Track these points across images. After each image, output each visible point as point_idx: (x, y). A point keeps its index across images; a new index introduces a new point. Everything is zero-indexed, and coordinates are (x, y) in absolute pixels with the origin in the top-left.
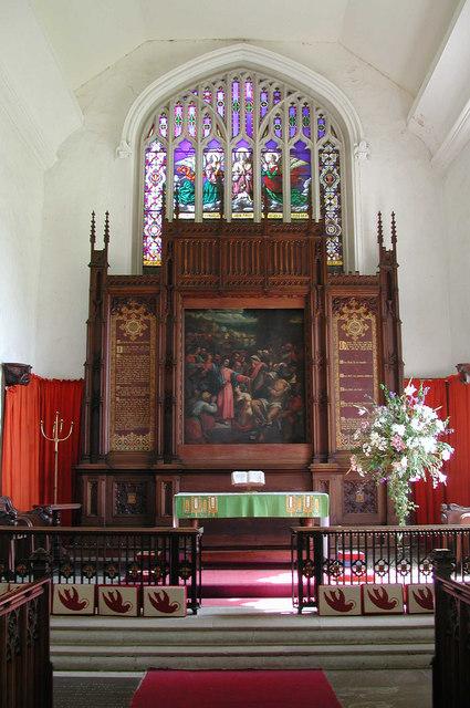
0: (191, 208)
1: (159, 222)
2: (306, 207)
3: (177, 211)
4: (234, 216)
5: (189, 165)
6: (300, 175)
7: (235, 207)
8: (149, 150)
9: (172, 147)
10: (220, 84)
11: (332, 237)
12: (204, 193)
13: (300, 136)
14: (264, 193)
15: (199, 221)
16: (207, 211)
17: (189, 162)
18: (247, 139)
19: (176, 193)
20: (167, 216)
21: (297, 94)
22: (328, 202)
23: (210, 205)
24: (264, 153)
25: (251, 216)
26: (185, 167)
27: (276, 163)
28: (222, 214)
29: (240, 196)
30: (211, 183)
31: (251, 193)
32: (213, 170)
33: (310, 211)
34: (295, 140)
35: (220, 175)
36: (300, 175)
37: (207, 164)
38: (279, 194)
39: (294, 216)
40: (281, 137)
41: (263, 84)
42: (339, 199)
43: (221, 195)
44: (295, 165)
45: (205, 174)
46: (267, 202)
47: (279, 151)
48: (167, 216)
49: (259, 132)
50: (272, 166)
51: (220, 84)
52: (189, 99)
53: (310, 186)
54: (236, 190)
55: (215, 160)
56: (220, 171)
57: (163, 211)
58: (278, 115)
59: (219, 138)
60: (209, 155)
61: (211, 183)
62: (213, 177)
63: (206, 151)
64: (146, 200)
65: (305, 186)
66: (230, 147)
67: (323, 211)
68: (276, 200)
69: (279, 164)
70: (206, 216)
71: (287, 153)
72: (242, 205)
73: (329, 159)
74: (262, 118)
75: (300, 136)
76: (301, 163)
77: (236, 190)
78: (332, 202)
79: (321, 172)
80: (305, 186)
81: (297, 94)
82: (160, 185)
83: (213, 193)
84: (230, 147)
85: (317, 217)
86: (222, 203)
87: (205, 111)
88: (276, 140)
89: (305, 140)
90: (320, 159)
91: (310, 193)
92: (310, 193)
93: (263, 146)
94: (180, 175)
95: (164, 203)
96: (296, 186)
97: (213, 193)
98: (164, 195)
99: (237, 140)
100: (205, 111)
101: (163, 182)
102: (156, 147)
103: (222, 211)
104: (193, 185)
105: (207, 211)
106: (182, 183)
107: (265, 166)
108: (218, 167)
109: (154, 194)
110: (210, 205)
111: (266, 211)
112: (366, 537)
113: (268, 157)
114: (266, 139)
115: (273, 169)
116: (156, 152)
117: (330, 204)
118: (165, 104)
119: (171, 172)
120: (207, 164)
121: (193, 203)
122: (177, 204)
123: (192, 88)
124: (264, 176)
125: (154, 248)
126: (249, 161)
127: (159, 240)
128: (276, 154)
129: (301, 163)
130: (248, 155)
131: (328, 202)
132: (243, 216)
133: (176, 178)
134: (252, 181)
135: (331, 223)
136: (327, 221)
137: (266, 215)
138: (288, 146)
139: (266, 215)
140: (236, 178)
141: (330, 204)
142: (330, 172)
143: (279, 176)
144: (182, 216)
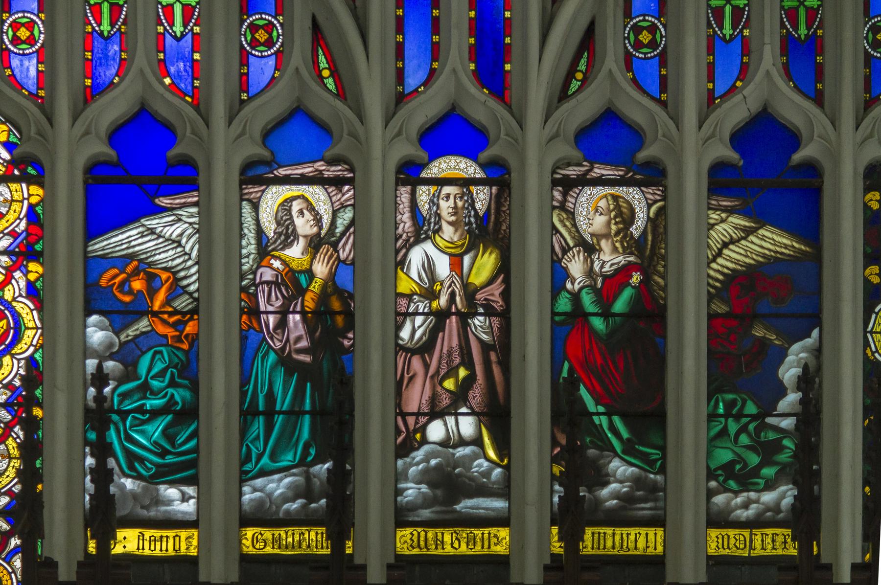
0: (178, 500)
2: (784, 495)
3: (104, 517)
4: (405, 540)
5: (166, 256)
6: (764, 309)
7: (412, 491)
12: (248, 413)
13: (768, 85)
14: (566, 415)
16: (263, 517)
17: (165, 237)
19: (98, 416)
23: (277, 486)
24: (568, 185)
25: (500, 541)
26: (139, 265)
27: (635, 246)
28: (337, 538)
29: (436, 431)
30: (286, 362)
31: (498, 418)
33: (805, 519)
34: (735, 113)
35: (334, 316)
36: (764, 309)
38: (649, 421)
39: (717, 542)
40: (664, 91)
43: (335, 432)
44: (735, 257)
45: (254, 312)
46: (578, 468)
47: (652, 175)
49: (536, 70)
50: (609, 258)
53: (808, 380)
54: (416, 397)
55: (304, 225)
56: (331, 286)
59: (324, 103)
61: (286, 362)
63: (256, 174)
64: (241, 265)
65: (789, 373)
66: (381, 166)
68: (629, 449)
69: (650, 251)
70: (255, 541)
71: (692, 181)
72: (450, 484)
75: (768, 85)
76: (772, 241)
77: (416, 397)
80: (789, 373)
83: (295, 413)
84: (381, 166)
86: (340, 479)
88: (637, 108)
89: (793, 108)
91: (810, 417)
92: (810, 417)
93: (567, 149)
94: (121, 317)
96: (740, 367)
97: (295, 413)
98: (31, 425)
103: (339, 518)
104: (187, 371)
105: (263, 517)
107: (576, 267)
108: (321, 269)
110: (277, 486)
111: (573, 517)
112: (141, 350)
113: (592, 210)
114: (583, 109)
115: (622, 275)
119: (67, 293)
120: (264, 251)
121: (186, 472)
122: (102, 476)
124: (569, 326)
126: (484, 232)
128: (634, 195)
129: (772, 241)
130: (482, 196)
132: (451, 543)
133: (97, 333)
134: (503, 347)
137: (572, 538)
138: (697, 146)
139: (572, 538)
140: (412, 331)
143: (651, 314)
144: (128, 541)
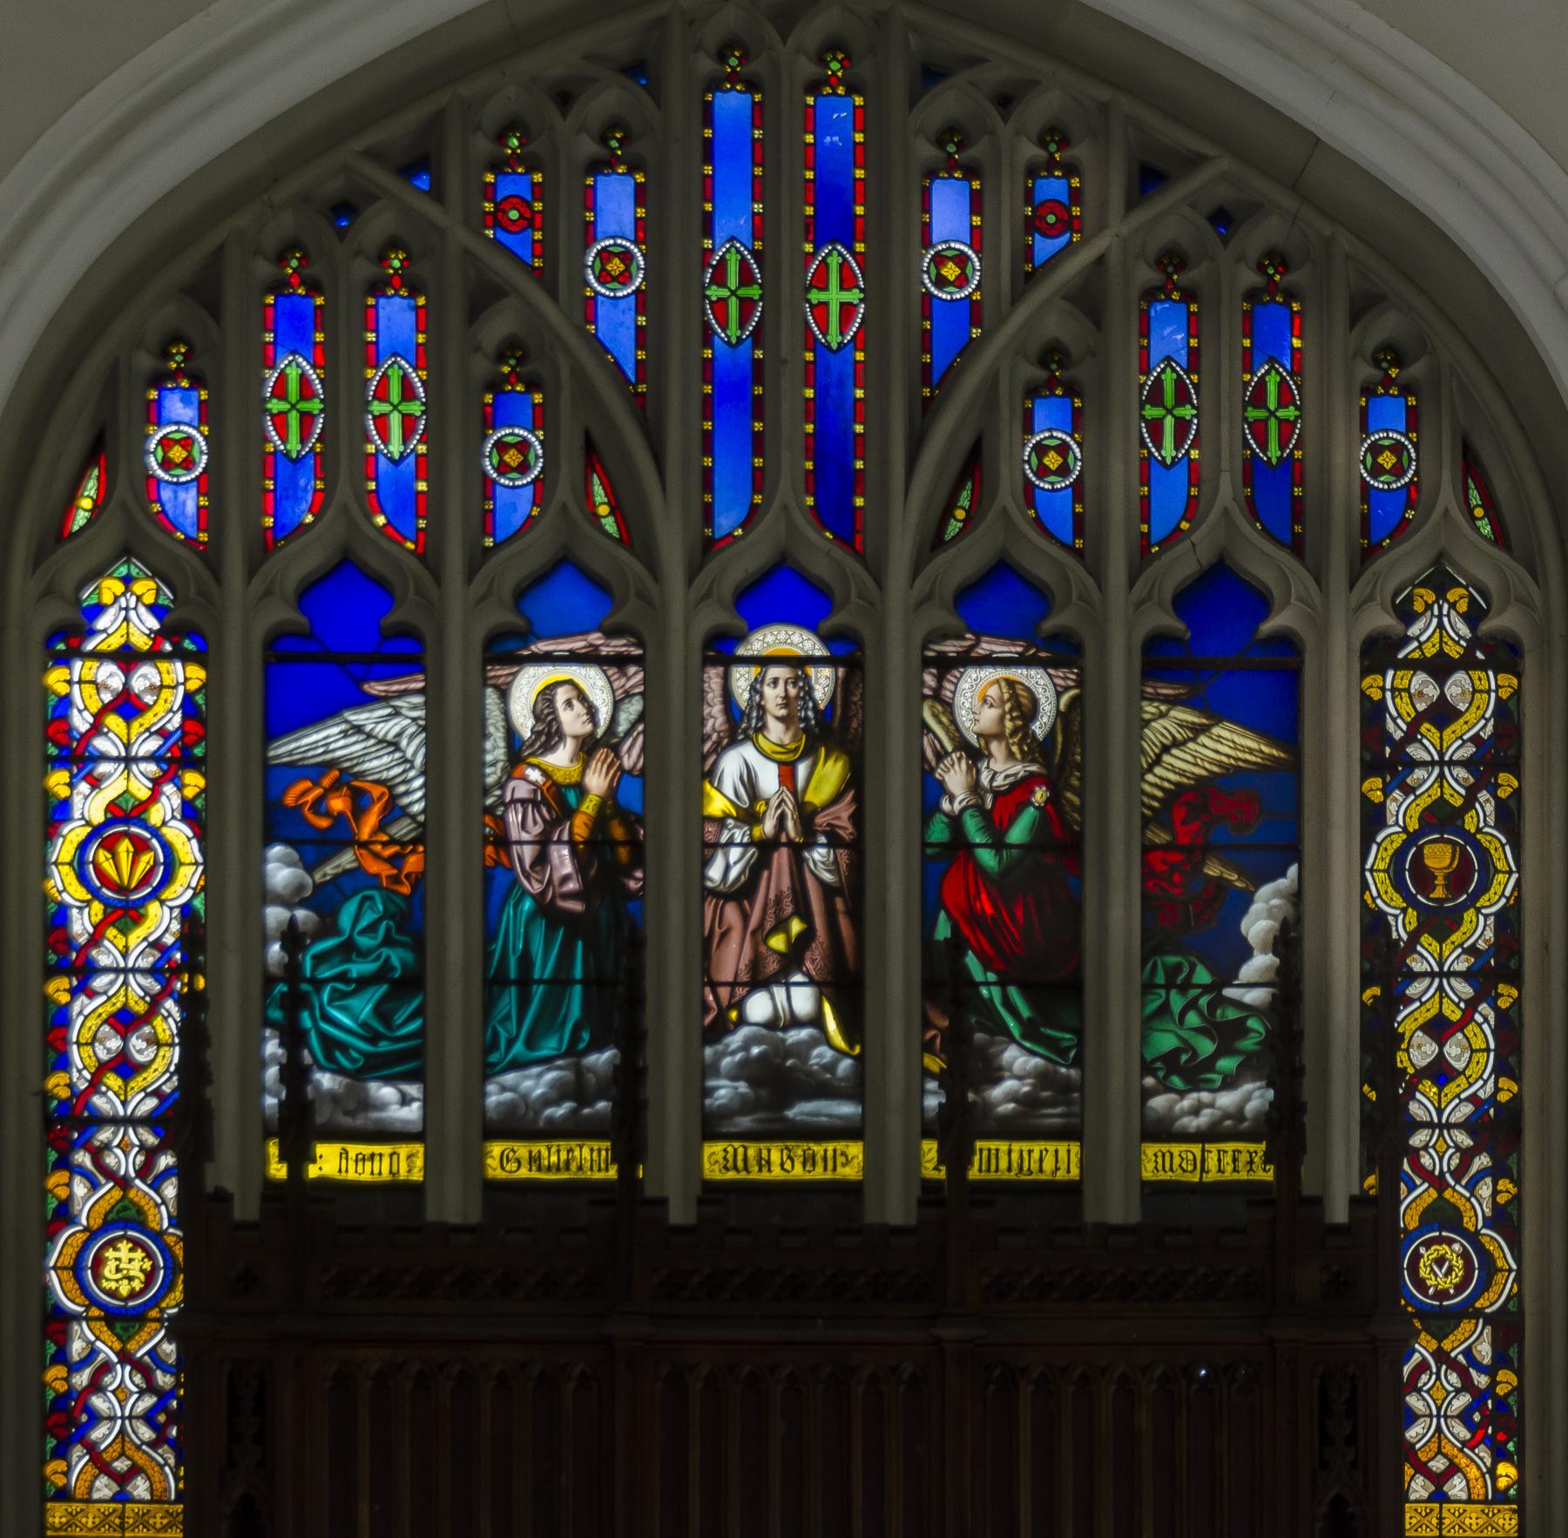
0: (397, 1103)
1: (161, 1203)
3: (300, 1127)
4: (716, 1160)
5: (379, 764)
7: (724, 1091)
8: (1380, 653)
9: (257, 612)
10: (609, 98)
11: (1443, 1320)
12: (494, 983)
15: (453, 1206)
16: (518, 1124)
18: (820, 553)
20: (223, 1173)
21: (1212, 180)
22: (1421, 1052)
23: (536, 1083)
25: (850, 1161)
26: (345, 777)
28: (628, 1152)
30: (546, 910)
31: (845, 987)
32: (557, 800)
37: (517, 754)
41: (945, 103)
42: (1508, 1029)
43: (619, 1007)
47: (1059, 652)
48: (223, 1173)
51: (609, 98)
52: (377, 224)
53: (1286, 941)
55: (572, 721)
56: (611, 805)
57: (183, 1122)
58: (1052, 354)
60: (528, 683)
62: (562, 860)
65: (1257, 925)
67: (1387, 1133)
68: (1031, 1032)
69: (1062, 757)
70: (504, 1160)
73: (1442, 714)
74: (925, 412)
78: (1453, 1050)
79: (1373, 817)
80: (1257, 925)
81: (1212, 180)
82: (1478, 929)
83: (559, 982)
85: (1342, 1177)
87: (498, 326)
90: (1373, 713)
91: (1288, 983)
94: (313, 847)
95: (193, 1069)
99: (741, 565)
100: (498, 326)
101: (1495, 898)
102: (1439, 628)
105: (518, 1124)
106: (325, 900)
107: (955, 778)
108: (597, 781)
109: (109, 993)
110: (536, 1083)
113: (976, 696)
115: (1018, 792)
116: (127, 658)
117: (1441, 1073)
118: (183, 268)
120: (517, 754)
121: (405, 1064)
123: (399, 127)
125: (121, 1404)
127: (153, 1341)
128: (1037, 680)
129: (1231, 744)
130: (823, 681)
131: (1421, 1052)
132: (781, 1163)
135: (1443, 1218)
136: (1414, 1201)
139: (957, 1157)
140: (726, 867)
141: (1441, 1073)
142: (1441, 818)
144: (328, 1161)
